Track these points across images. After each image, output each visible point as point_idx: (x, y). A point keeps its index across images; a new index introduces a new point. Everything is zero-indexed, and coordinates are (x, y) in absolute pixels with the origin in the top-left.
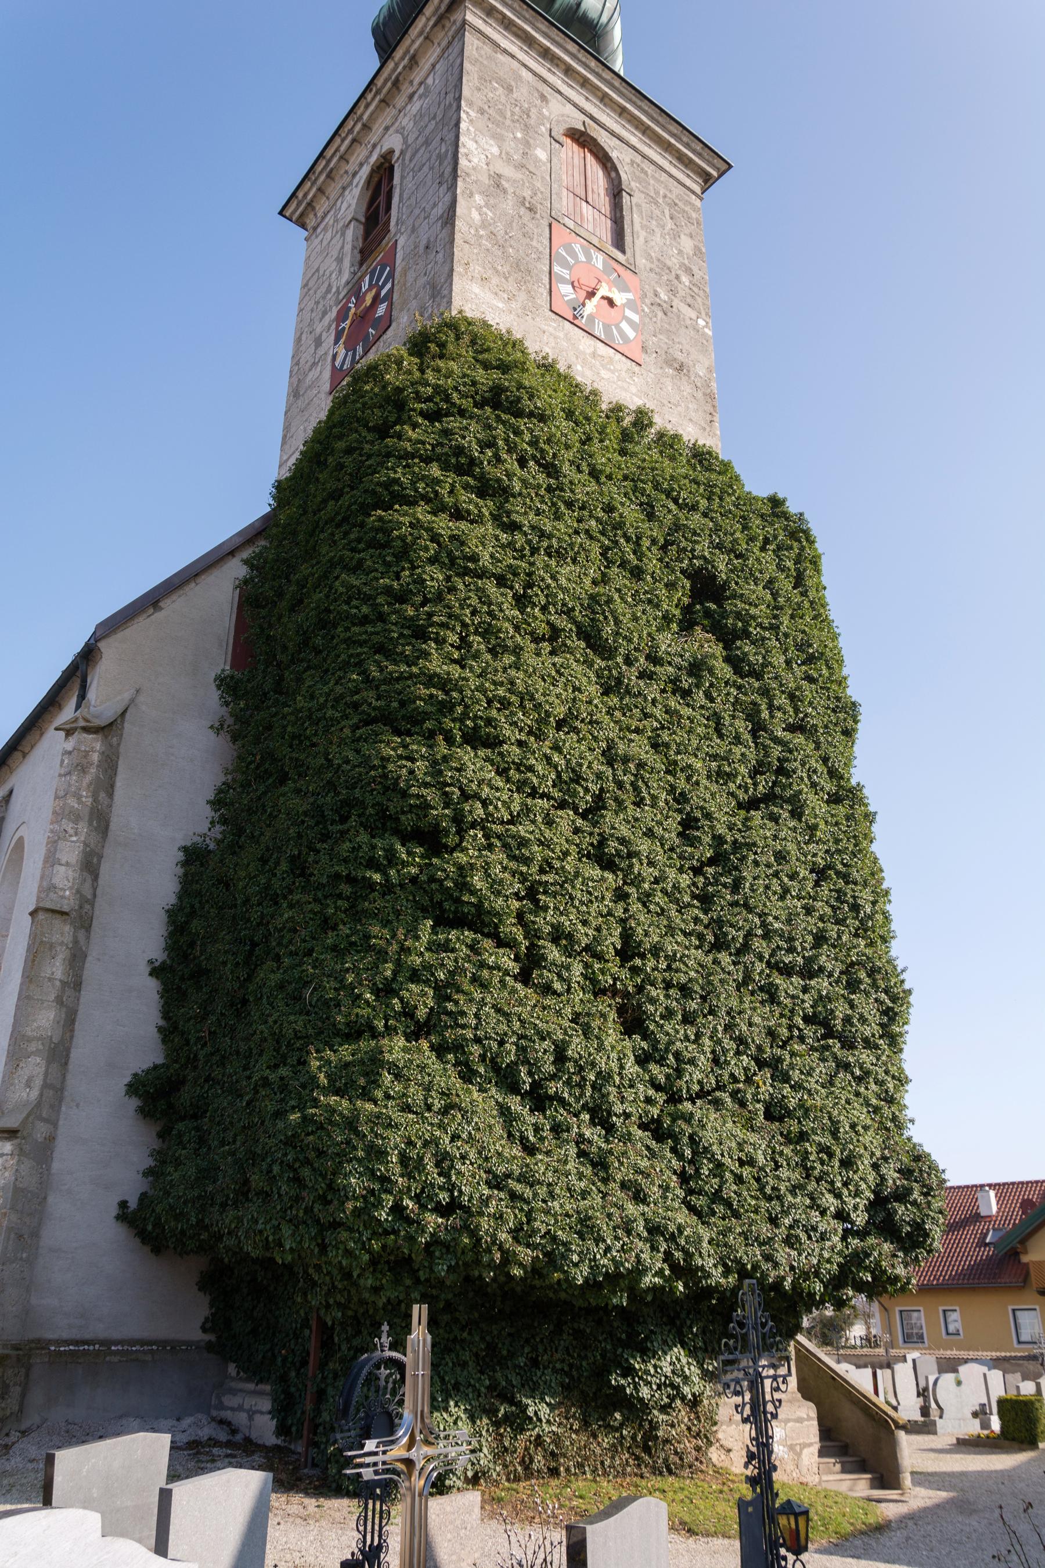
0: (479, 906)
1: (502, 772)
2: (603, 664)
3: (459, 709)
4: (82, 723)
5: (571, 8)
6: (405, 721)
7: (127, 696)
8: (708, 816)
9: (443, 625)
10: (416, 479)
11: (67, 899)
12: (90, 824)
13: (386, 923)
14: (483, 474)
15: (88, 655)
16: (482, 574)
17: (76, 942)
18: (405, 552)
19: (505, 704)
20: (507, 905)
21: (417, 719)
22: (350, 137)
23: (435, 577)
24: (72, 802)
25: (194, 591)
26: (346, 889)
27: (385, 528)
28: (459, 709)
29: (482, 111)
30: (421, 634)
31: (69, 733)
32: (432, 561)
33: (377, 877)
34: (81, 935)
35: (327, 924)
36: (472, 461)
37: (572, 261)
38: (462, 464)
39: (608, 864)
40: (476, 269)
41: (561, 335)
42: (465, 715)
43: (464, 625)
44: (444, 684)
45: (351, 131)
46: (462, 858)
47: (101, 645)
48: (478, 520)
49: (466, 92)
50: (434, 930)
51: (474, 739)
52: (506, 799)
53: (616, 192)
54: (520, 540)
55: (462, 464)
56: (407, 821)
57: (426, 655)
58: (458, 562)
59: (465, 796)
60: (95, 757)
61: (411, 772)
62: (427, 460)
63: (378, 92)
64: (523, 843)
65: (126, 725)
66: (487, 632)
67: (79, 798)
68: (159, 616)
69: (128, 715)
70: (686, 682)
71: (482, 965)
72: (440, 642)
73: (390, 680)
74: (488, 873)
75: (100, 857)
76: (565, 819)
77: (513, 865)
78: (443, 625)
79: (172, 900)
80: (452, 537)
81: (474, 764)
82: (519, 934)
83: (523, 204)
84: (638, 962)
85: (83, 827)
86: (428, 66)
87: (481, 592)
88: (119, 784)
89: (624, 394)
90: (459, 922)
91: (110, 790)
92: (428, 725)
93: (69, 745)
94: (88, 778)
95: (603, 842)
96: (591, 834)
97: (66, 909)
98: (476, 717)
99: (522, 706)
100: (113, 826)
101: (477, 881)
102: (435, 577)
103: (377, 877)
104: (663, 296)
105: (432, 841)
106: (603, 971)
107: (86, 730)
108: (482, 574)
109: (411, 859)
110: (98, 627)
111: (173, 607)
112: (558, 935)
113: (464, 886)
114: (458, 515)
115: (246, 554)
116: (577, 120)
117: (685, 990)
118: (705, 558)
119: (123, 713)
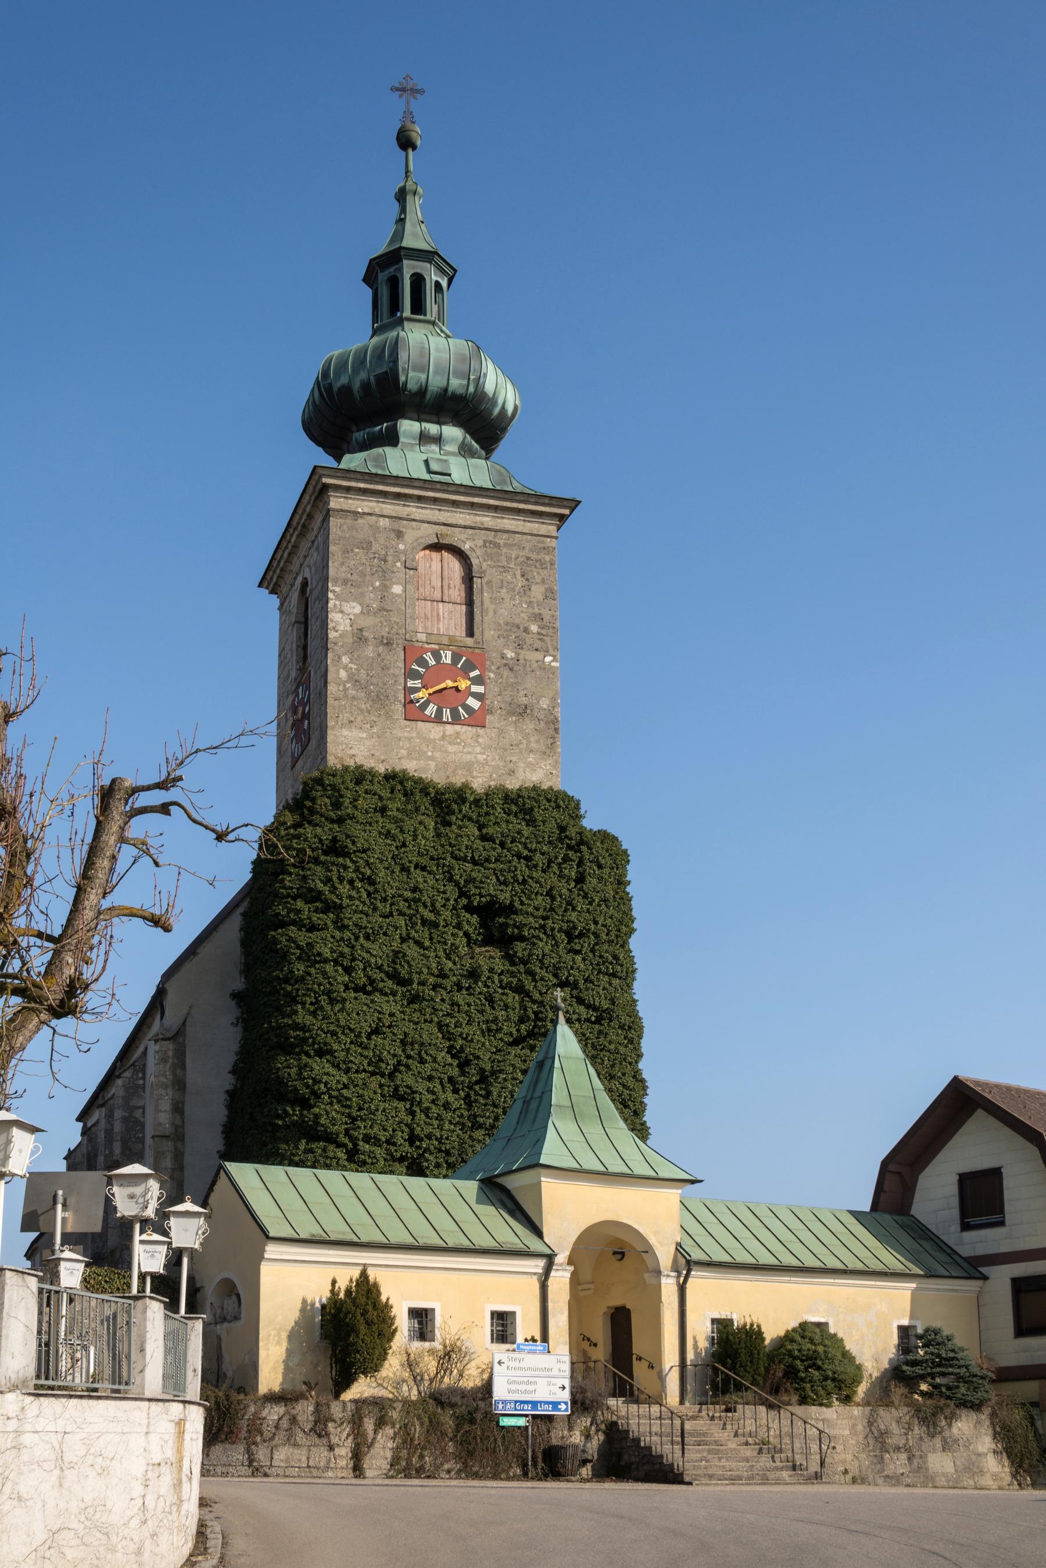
0: (326, 1131)
1: (337, 1067)
2: (405, 990)
3: (310, 1041)
4: (161, 1036)
5: (440, 394)
6: (288, 1048)
7: (184, 1012)
8: (478, 1058)
9: (304, 995)
10: (290, 911)
11: (167, 1128)
12: (173, 1088)
13: (287, 1143)
14: (326, 900)
15: (160, 993)
16: (326, 961)
17: (176, 1148)
18: (285, 955)
19: (334, 1034)
20: (339, 1128)
21: (293, 1046)
22: (296, 533)
23: (299, 968)
24: (163, 1079)
25: (216, 937)
26: (270, 1128)
27: (275, 941)
28: (310, 1041)
29: (345, 582)
30: (294, 1000)
31: (156, 1041)
32: (299, 958)
33: (280, 1123)
34: (179, 1145)
35: (265, 1145)
36: (320, 893)
37: (422, 670)
38: (313, 897)
39: (401, 1098)
40: (346, 716)
41: (414, 734)
42: (314, 1043)
43: (315, 992)
44: (304, 1028)
45: (286, 547)
46: (316, 1110)
47: (167, 986)
48: (325, 928)
49: (332, 572)
50: (307, 1144)
51: (320, 1053)
52: (336, 1077)
53: (468, 579)
54: (347, 934)
55: (313, 897)
56: (291, 1096)
57: (296, 1012)
58: (309, 956)
59: (316, 1081)
60: (170, 1053)
61: (289, 1074)
62: (295, 898)
63: (295, 529)
64: (348, 1099)
65: (187, 1028)
66: (328, 993)
67: (165, 1076)
68: (197, 958)
69: (187, 1023)
70: (465, 983)
71: (327, 1157)
72: (303, 1004)
73: (279, 1027)
74: (329, 1115)
75: (183, 1103)
76: (374, 1082)
77: (342, 1110)
78: (304, 995)
79: (225, 1119)
80: (308, 944)
81: (319, 1066)
82: (346, 1141)
83: (382, 643)
84: (418, 1143)
85: (170, 1092)
86: (316, 528)
87: (324, 973)
88: (188, 1060)
89: (469, 757)
90: (318, 1139)
91: (183, 1066)
92: (297, 1050)
93: (157, 1048)
94: (168, 1065)
95: (396, 1089)
96: (389, 1086)
97: (167, 1134)
98: (319, 1043)
99: (343, 1033)
100: (188, 1085)
101: (322, 1121)
102: (299, 968)
103: (280, 1123)
104: (510, 654)
105: (305, 1104)
106: (396, 1151)
107: (163, 1039)
108: (326, 961)
109: (294, 1113)
110: (163, 976)
111: (204, 951)
112: (367, 1139)
113: (317, 1123)
114: (312, 928)
115: (241, 910)
116: (429, 532)
117: (447, 1153)
118: (490, 895)
119: (184, 1023)
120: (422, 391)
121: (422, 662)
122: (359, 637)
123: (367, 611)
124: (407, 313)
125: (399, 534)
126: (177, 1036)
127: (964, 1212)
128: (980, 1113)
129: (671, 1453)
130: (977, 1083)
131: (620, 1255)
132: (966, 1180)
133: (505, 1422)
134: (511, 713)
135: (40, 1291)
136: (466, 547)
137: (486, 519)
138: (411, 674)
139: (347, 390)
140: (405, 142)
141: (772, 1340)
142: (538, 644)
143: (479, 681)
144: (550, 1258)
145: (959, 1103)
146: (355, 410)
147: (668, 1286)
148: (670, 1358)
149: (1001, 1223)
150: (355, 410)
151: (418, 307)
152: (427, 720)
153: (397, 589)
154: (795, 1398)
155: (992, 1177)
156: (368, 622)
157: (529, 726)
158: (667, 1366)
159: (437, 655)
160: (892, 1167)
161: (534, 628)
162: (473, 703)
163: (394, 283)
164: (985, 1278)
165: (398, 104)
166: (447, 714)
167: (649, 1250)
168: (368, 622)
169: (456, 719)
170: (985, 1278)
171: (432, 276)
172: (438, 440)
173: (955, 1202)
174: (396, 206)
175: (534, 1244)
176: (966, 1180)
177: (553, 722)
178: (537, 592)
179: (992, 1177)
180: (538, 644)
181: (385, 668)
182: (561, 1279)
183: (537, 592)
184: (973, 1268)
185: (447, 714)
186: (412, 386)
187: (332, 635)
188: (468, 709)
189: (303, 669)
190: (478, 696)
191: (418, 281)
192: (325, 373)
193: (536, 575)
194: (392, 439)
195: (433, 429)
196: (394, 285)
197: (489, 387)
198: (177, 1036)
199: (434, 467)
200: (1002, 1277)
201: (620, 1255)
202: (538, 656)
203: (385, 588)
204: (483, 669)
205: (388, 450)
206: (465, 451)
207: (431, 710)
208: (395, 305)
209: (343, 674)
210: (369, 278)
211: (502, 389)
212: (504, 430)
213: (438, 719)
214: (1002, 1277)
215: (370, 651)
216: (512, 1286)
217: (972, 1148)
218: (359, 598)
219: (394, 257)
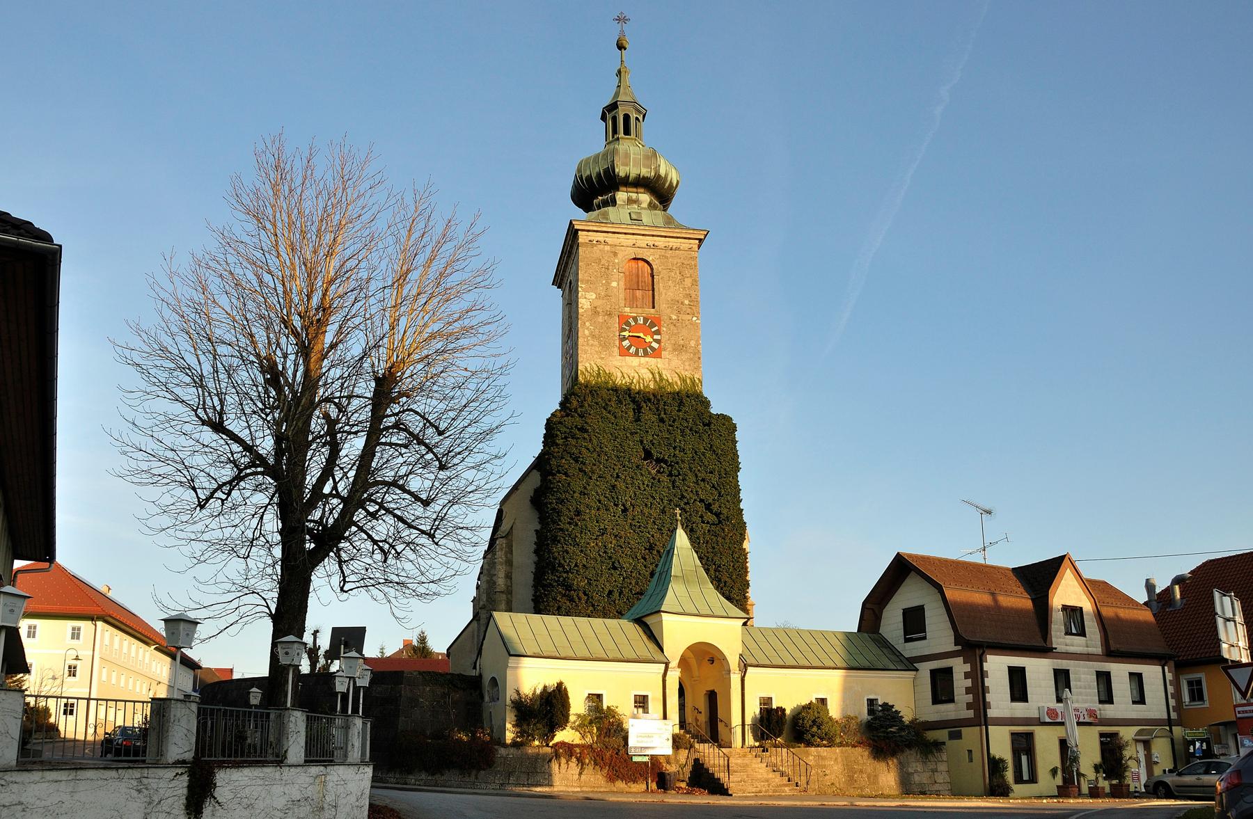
49: (580, 276)
91: (511, 552)
104: (674, 317)
111: (522, 488)
120: (627, 177)
121: (628, 324)
122: (595, 311)
123: (599, 297)
124: (621, 134)
125: (615, 254)
126: (508, 535)
127: (906, 632)
128: (913, 573)
129: (722, 776)
130: (910, 556)
131: (712, 661)
132: (907, 613)
133: (635, 759)
134: (675, 350)
135: (199, 709)
136: (650, 259)
137: (661, 242)
138: (646, 320)
139: (589, 178)
140: (621, 47)
141: (792, 710)
142: (689, 311)
143: (658, 332)
144: (667, 664)
145: (901, 570)
146: (594, 190)
147: (735, 679)
148: (736, 720)
149: (925, 638)
150: (594, 190)
151: (627, 132)
152: (631, 355)
153: (614, 284)
154: (595, 746)
155: (920, 609)
156: (599, 302)
157: (685, 356)
158: (733, 725)
159: (635, 319)
160: (868, 606)
161: (687, 302)
162: (655, 345)
163: (614, 119)
164: (917, 670)
165: (617, 27)
166: (641, 351)
167: (725, 659)
168: (599, 302)
169: (646, 354)
170: (917, 670)
171: (633, 115)
172: (636, 201)
173: (901, 625)
174: (617, 79)
175: (658, 656)
176: (907, 613)
177: (696, 352)
178: (688, 282)
179: (920, 609)
180: (689, 311)
181: (608, 328)
182: (674, 676)
183: (688, 282)
184: (910, 664)
185: (641, 351)
186: (622, 174)
187: (580, 311)
188: (653, 349)
189: (570, 330)
190: (658, 341)
191: (627, 118)
192: (579, 170)
193: (687, 273)
194: (613, 202)
195: (634, 196)
196: (618, 120)
197: (662, 172)
198: (508, 535)
199: (634, 216)
200: (926, 668)
201: (712, 661)
202: (689, 317)
203: (609, 284)
204: (660, 326)
205: (610, 208)
206: (651, 206)
207: (633, 350)
208: (615, 131)
209: (587, 332)
210: (604, 118)
211: (668, 171)
212: (673, 195)
213: (636, 354)
214: (926, 668)
215: (600, 319)
216: (646, 678)
217: (910, 595)
218: (594, 290)
219: (613, 107)
